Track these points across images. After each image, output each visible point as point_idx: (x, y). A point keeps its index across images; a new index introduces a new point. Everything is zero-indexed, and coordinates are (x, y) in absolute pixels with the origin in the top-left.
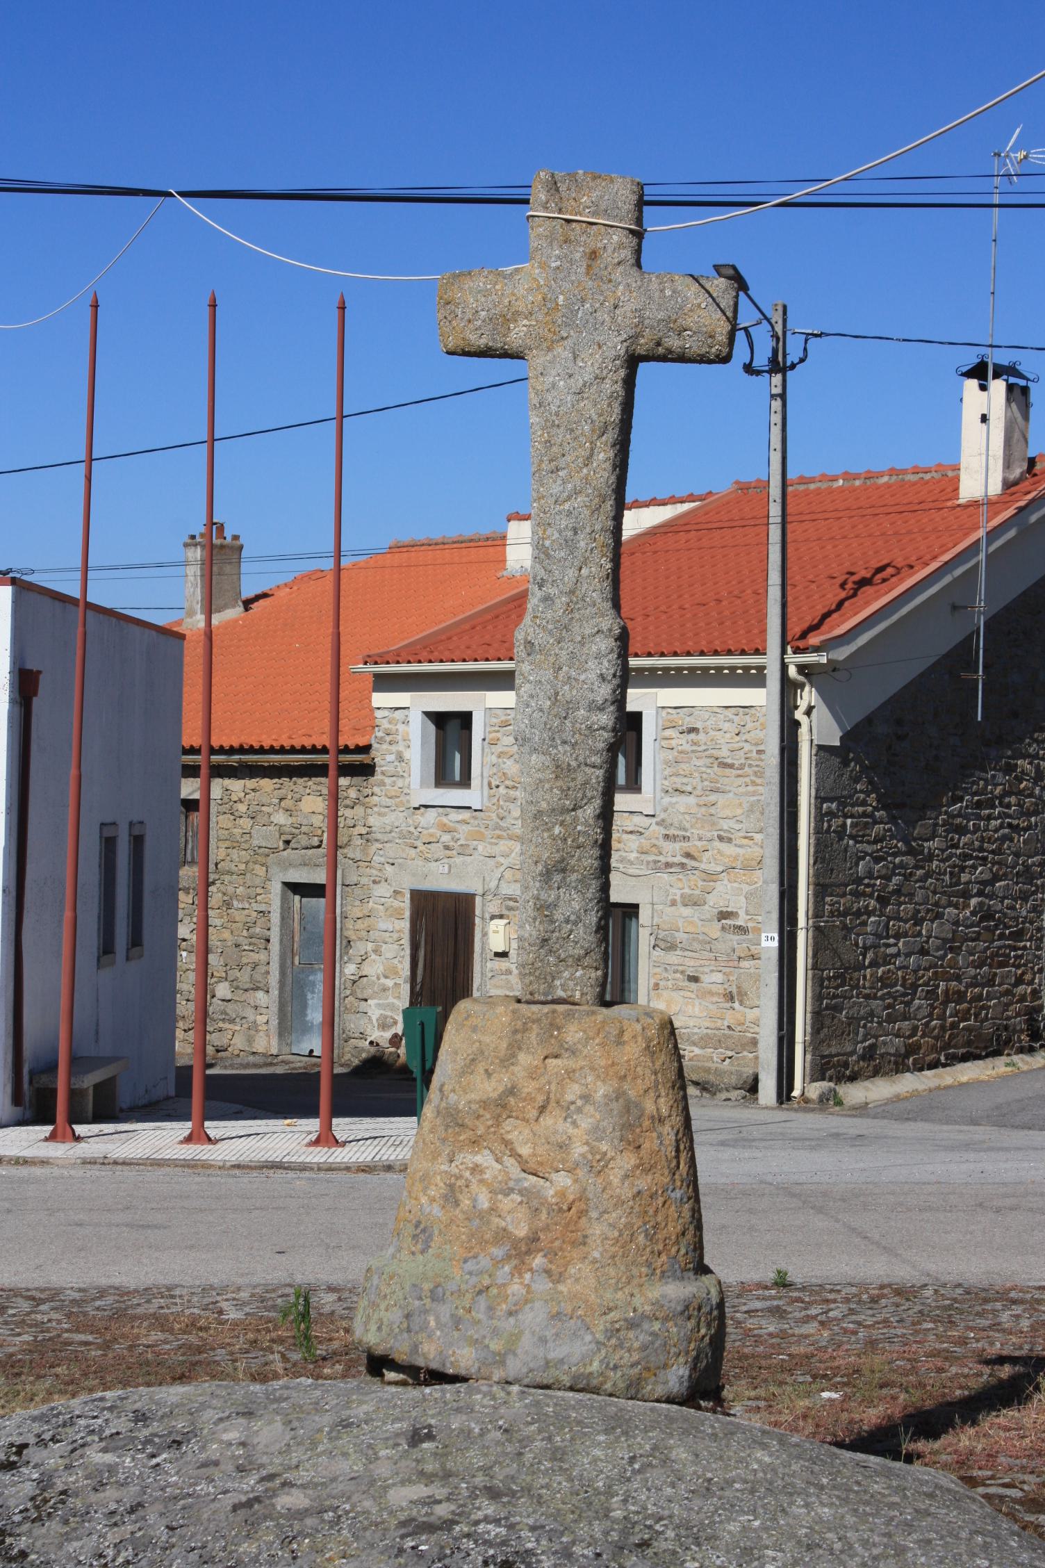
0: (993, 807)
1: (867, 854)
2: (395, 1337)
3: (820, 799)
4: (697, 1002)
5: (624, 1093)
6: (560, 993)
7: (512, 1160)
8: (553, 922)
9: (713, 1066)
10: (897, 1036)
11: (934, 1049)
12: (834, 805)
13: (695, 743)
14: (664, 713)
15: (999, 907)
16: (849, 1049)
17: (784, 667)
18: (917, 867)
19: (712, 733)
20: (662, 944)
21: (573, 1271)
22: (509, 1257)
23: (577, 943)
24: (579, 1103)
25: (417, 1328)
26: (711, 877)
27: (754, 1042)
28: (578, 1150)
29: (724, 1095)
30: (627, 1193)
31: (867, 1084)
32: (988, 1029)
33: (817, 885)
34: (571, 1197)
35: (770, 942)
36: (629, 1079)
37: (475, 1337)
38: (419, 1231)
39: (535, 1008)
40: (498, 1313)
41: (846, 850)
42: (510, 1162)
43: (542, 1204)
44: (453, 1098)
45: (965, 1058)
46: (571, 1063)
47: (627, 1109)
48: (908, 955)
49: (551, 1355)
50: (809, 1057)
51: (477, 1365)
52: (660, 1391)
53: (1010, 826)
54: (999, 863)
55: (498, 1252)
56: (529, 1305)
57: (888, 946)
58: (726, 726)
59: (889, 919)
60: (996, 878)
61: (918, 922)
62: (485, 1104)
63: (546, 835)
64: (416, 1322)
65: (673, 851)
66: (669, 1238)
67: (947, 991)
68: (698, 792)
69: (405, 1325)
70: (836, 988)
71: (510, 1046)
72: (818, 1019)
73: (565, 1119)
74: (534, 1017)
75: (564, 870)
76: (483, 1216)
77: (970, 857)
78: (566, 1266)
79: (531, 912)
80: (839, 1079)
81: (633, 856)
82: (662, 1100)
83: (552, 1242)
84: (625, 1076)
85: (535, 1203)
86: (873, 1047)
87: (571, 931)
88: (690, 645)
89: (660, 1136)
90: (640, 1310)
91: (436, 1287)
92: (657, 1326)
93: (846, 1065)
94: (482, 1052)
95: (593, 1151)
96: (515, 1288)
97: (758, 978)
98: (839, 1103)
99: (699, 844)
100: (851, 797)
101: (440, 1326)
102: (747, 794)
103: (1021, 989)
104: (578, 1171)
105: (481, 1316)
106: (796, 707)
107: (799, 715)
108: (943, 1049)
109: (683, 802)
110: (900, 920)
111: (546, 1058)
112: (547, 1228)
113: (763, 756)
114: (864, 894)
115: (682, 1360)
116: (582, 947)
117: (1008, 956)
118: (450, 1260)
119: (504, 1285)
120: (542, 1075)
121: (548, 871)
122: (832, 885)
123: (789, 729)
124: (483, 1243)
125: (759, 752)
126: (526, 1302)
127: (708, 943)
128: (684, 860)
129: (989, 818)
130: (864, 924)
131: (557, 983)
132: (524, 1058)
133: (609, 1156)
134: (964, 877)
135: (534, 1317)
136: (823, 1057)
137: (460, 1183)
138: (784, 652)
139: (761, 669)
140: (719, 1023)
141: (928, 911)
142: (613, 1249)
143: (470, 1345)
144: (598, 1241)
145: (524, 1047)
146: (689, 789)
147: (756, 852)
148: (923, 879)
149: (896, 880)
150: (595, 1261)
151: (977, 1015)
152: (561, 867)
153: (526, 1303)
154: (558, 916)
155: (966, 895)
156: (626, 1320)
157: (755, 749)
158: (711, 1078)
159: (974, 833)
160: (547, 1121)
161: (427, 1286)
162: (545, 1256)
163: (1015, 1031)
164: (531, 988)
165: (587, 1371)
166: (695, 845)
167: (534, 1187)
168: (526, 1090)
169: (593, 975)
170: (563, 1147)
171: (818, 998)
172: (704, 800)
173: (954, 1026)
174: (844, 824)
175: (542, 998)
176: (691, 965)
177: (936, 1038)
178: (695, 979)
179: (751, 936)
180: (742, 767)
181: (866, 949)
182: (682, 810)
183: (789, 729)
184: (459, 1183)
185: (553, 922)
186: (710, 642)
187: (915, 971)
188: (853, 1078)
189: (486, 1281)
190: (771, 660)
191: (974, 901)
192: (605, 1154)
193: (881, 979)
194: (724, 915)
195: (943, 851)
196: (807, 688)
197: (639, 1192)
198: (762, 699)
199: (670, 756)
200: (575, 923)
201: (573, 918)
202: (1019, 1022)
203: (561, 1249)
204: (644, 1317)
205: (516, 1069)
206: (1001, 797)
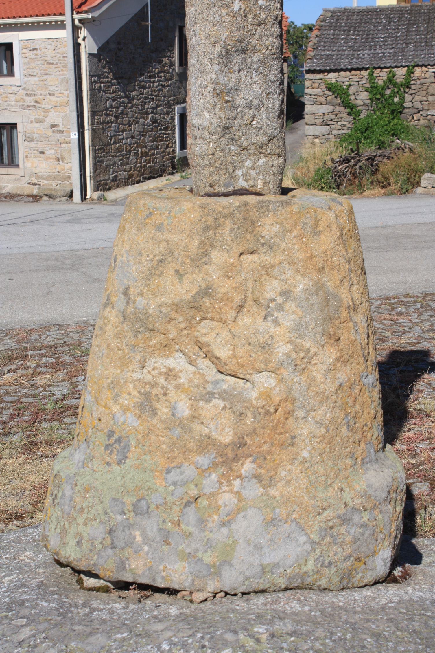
0: (155, 78)
1: (110, 98)
2: (98, 554)
3: (91, 76)
4: (44, 162)
5: (323, 286)
6: (242, 184)
7: (207, 362)
8: (234, 108)
9: (53, 188)
10: (125, 171)
11: (138, 175)
12: (96, 78)
13: (36, 55)
14: (22, 42)
15: (159, 118)
16: (107, 177)
17: (73, 20)
18: (129, 103)
19: (43, 50)
20: (28, 139)
21: (283, 473)
22: (215, 465)
23: (259, 129)
24: (280, 300)
25: (122, 544)
26: (47, 110)
27: (69, 177)
28: (282, 349)
29: (59, 199)
30: (330, 387)
31: (115, 191)
32: (157, 166)
33: (92, 111)
34: (277, 399)
35: (74, 136)
36: (327, 270)
37: (188, 551)
38: (112, 440)
39: (223, 200)
40: (210, 525)
41: (102, 97)
42: (204, 364)
43: (247, 408)
44: (141, 302)
45: (150, 178)
46: (269, 258)
47: (327, 302)
48: (127, 139)
49: (267, 560)
50: (92, 182)
51: (190, 578)
52: (369, 577)
53: (162, 85)
54: (158, 100)
55: (203, 460)
56: (242, 514)
57: (119, 135)
58: (49, 47)
59: (120, 124)
60: (158, 106)
61: (130, 125)
62: (177, 307)
63: (224, 12)
64: (121, 538)
65: (30, 100)
66: (366, 425)
67: (142, 152)
68: (39, 75)
69: (109, 541)
70: (101, 153)
71: (202, 244)
72: (95, 166)
73: (265, 317)
74: (226, 211)
75: (244, 51)
76: (185, 425)
77: (148, 98)
78: (276, 469)
79: (209, 97)
80: (104, 190)
81: (13, 103)
82: (355, 288)
83: (260, 446)
84: (323, 268)
85: (239, 407)
86: (116, 176)
87: (254, 117)
88: (31, 13)
89: (355, 324)
90: (351, 504)
91: (139, 501)
92: (366, 517)
93: (106, 184)
94: (171, 252)
95: (297, 348)
96: (226, 498)
97: (70, 151)
98: (105, 200)
99: (41, 97)
100: (102, 74)
101: (146, 540)
102: (60, 75)
103: (168, 150)
104: (282, 370)
105: (191, 529)
106: (79, 37)
107: (80, 41)
108: (142, 175)
109: (33, 80)
110: (123, 124)
111: (241, 254)
112: (254, 432)
113: (66, 59)
114: (109, 115)
115: (386, 543)
116: (265, 134)
117: (163, 137)
118: (152, 471)
119: (213, 495)
120: (238, 273)
121: (228, 51)
122: (97, 111)
123: (77, 46)
124: (186, 452)
125: (64, 57)
126: (239, 510)
127: (47, 138)
128: (35, 104)
129: (154, 82)
130: (110, 127)
131: (239, 172)
132: (216, 255)
133: (313, 351)
134: (146, 106)
135: (248, 525)
136: (98, 182)
137: (157, 391)
138: (72, 14)
139: (62, 22)
140: (54, 170)
141: (134, 121)
142: (321, 446)
143: (182, 560)
144: (307, 441)
145: (218, 244)
146: (35, 74)
147: (66, 99)
148: (131, 108)
149: (121, 108)
150: (304, 461)
151: (153, 161)
152: (242, 48)
153: (238, 513)
154: (240, 101)
155: (147, 113)
156: (339, 517)
157: (62, 56)
158: (53, 193)
159: (149, 88)
160: (245, 320)
161: (129, 500)
162: (254, 461)
163: (167, 167)
164: (211, 180)
165: (302, 571)
166: (39, 98)
167: (235, 389)
168: (222, 290)
169: (275, 163)
170: (266, 347)
171: (95, 158)
172: (41, 78)
173: (145, 166)
174: (100, 86)
175: (223, 190)
176: (41, 148)
177: (139, 171)
178: (43, 153)
179: (65, 134)
180: (57, 64)
181: (111, 137)
182: (33, 83)
183: (77, 46)
184: (155, 391)
185: (234, 108)
186: (39, 11)
187: (130, 145)
188: (109, 189)
189: (194, 492)
190: (67, 18)
191: (150, 116)
192: (309, 350)
193: (117, 149)
194: (53, 126)
195: (138, 96)
196: (83, 29)
197: (340, 386)
198: (64, 35)
199: (26, 60)
200: (258, 108)
201: (255, 102)
202: (168, 163)
203: (270, 452)
204: (355, 510)
205: (210, 268)
206: (158, 73)
